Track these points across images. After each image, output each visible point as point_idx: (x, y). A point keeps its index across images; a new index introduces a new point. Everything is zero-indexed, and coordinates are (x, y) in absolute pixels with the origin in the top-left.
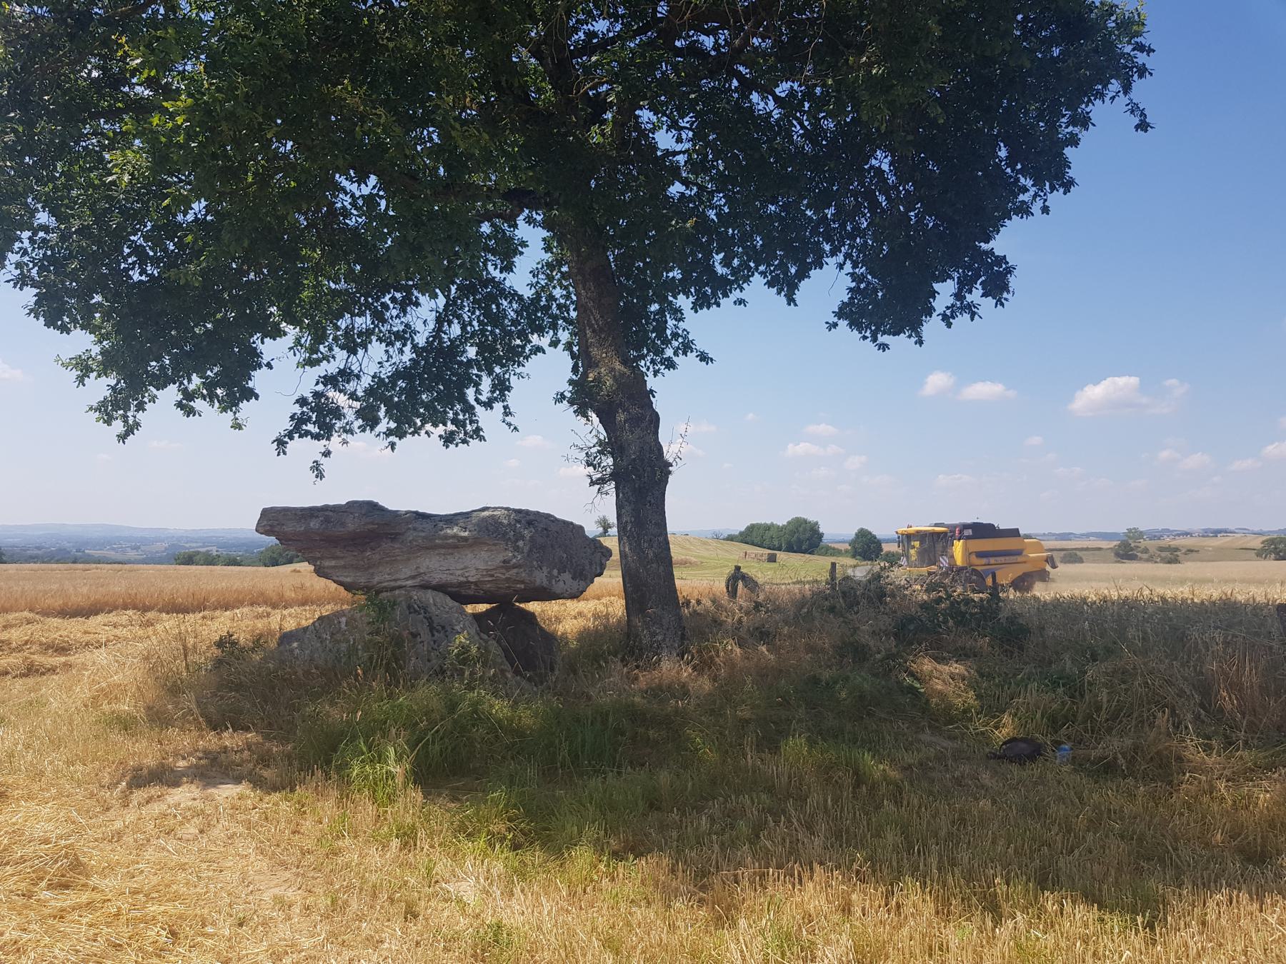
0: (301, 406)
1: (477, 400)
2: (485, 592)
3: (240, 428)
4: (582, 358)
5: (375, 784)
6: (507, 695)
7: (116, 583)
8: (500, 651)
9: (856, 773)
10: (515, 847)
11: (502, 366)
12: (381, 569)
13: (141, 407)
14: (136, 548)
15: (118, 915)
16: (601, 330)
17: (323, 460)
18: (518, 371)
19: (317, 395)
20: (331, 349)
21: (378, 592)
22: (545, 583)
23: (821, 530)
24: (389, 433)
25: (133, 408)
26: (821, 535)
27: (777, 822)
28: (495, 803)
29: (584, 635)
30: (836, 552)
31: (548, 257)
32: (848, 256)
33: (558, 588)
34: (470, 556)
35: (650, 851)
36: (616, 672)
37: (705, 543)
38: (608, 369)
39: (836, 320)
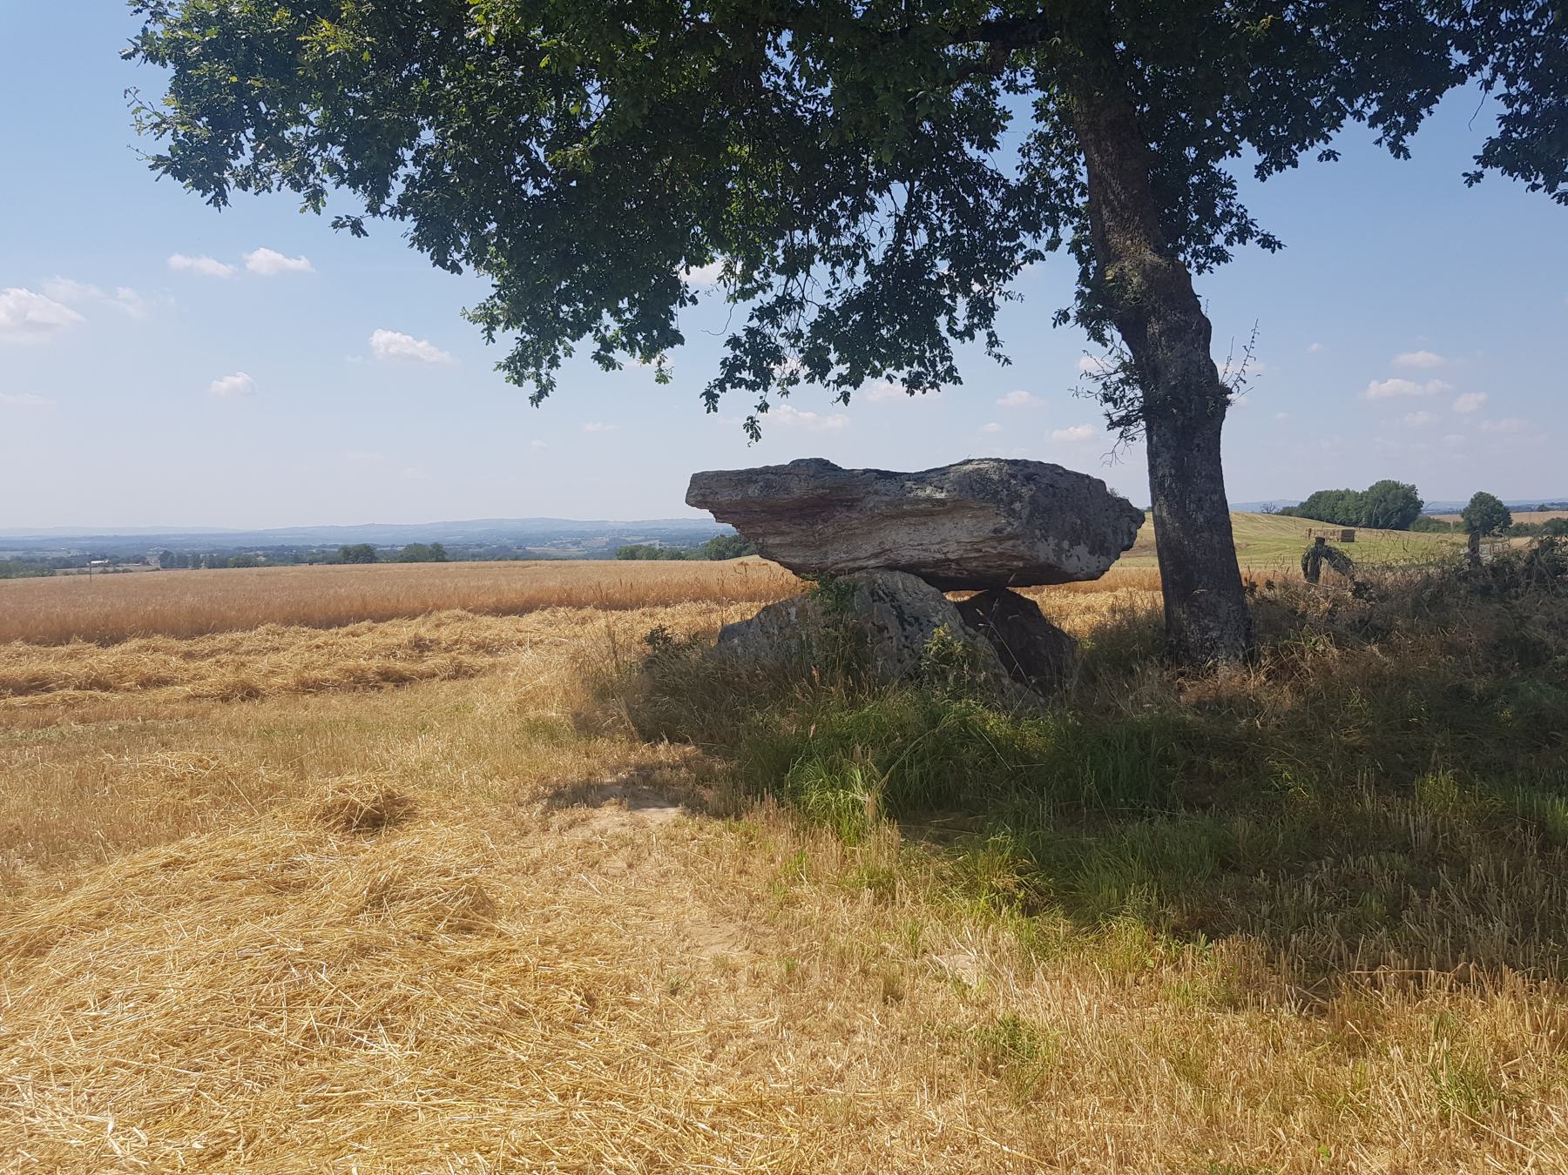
0: (733, 349)
1: (951, 330)
2: (970, 573)
3: (666, 381)
4: (1094, 252)
5: (839, 815)
6: (1005, 707)
7: (550, 578)
8: (991, 650)
9: (1542, 827)
10: (1029, 910)
11: (983, 283)
12: (836, 545)
13: (554, 362)
14: (577, 544)
15: (525, 970)
16: (1124, 207)
17: (760, 416)
18: (1004, 289)
19: (751, 332)
20: (767, 275)
21: (833, 577)
22: (1052, 559)
23: (1419, 498)
24: (841, 381)
25: (545, 364)
26: (1419, 505)
27: (1425, 897)
28: (1000, 848)
29: (1099, 633)
30: (1441, 527)
31: (1043, 127)
32: (1498, 68)
33: (1070, 565)
34: (949, 525)
35: (1230, 931)
36: (1153, 677)
37: (1251, 520)
38: (1136, 260)
39: (1479, 168)
